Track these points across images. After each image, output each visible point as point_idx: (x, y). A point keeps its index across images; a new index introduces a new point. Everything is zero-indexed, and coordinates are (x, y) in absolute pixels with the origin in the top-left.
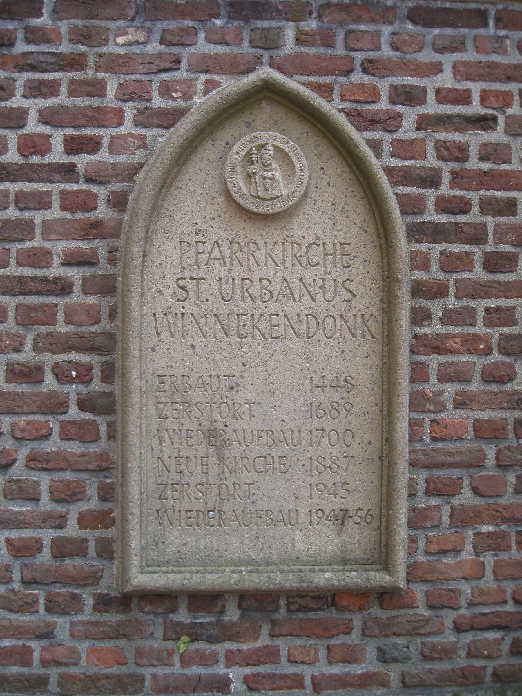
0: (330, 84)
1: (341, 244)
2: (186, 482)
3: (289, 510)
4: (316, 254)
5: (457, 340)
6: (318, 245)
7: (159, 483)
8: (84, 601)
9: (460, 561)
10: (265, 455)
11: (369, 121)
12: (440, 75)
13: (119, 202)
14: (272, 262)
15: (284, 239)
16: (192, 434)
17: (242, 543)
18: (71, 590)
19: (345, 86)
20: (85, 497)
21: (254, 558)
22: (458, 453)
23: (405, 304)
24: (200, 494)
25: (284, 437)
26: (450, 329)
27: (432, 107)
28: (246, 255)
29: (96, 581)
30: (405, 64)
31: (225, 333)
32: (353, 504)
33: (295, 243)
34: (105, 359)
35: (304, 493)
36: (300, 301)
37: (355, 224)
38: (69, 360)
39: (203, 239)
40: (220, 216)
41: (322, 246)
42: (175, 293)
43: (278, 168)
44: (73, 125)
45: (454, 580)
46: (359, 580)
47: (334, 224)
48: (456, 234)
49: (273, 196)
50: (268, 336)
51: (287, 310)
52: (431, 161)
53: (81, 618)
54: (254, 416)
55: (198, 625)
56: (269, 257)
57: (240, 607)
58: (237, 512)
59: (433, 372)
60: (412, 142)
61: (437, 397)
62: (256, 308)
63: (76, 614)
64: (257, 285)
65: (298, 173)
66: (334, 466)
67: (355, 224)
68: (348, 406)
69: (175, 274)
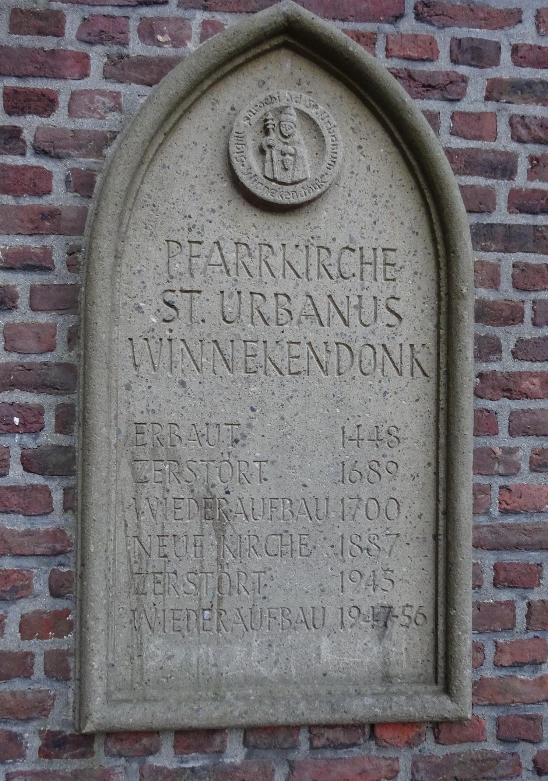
0: (372, 33)
1: (384, 250)
2: (173, 571)
3: (313, 608)
4: (351, 262)
5: (536, 381)
6: (353, 250)
7: (135, 571)
8: (27, 743)
9: (541, 678)
10: (280, 532)
11: (424, 86)
12: (519, 27)
13: (83, 184)
14: (292, 271)
15: (308, 241)
16: (182, 504)
17: (249, 654)
18: (8, 728)
19: (393, 38)
20: (30, 594)
21: (266, 675)
22: (537, 531)
23: (469, 330)
24: (192, 587)
25: (307, 507)
26: (526, 366)
27: (506, 70)
28: (256, 262)
29: (44, 713)
30: (472, 10)
31: (228, 366)
32: (398, 598)
33: (323, 247)
34: (64, 399)
35: (334, 584)
36: (329, 325)
37: (402, 223)
38: (10, 401)
39: (198, 238)
40: (221, 207)
41: (358, 251)
42: (159, 311)
43: (303, 142)
44: (17, 73)
45: (533, 704)
46: (411, 709)
47: (375, 223)
48: (534, 241)
49: (295, 179)
50: (285, 371)
51: (311, 337)
52: (504, 143)
53: (21, 766)
54: (265, 480)
55: (188, 772)
56: (287, 264)
57: (246, 743)
58: (242, 611)
59: (503, 423)
60: (479, 116)
61: (508, 456)
62: (270, 333)
63: (15, 761)
64: (272, 301)
65: (329, 148)
66: (373, 547)
67: (402, 223)
68: (392, 467)
69: (159, 285)
